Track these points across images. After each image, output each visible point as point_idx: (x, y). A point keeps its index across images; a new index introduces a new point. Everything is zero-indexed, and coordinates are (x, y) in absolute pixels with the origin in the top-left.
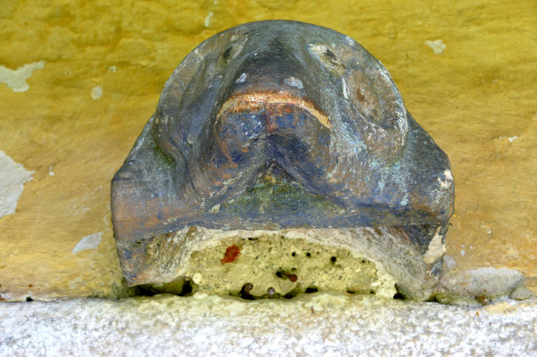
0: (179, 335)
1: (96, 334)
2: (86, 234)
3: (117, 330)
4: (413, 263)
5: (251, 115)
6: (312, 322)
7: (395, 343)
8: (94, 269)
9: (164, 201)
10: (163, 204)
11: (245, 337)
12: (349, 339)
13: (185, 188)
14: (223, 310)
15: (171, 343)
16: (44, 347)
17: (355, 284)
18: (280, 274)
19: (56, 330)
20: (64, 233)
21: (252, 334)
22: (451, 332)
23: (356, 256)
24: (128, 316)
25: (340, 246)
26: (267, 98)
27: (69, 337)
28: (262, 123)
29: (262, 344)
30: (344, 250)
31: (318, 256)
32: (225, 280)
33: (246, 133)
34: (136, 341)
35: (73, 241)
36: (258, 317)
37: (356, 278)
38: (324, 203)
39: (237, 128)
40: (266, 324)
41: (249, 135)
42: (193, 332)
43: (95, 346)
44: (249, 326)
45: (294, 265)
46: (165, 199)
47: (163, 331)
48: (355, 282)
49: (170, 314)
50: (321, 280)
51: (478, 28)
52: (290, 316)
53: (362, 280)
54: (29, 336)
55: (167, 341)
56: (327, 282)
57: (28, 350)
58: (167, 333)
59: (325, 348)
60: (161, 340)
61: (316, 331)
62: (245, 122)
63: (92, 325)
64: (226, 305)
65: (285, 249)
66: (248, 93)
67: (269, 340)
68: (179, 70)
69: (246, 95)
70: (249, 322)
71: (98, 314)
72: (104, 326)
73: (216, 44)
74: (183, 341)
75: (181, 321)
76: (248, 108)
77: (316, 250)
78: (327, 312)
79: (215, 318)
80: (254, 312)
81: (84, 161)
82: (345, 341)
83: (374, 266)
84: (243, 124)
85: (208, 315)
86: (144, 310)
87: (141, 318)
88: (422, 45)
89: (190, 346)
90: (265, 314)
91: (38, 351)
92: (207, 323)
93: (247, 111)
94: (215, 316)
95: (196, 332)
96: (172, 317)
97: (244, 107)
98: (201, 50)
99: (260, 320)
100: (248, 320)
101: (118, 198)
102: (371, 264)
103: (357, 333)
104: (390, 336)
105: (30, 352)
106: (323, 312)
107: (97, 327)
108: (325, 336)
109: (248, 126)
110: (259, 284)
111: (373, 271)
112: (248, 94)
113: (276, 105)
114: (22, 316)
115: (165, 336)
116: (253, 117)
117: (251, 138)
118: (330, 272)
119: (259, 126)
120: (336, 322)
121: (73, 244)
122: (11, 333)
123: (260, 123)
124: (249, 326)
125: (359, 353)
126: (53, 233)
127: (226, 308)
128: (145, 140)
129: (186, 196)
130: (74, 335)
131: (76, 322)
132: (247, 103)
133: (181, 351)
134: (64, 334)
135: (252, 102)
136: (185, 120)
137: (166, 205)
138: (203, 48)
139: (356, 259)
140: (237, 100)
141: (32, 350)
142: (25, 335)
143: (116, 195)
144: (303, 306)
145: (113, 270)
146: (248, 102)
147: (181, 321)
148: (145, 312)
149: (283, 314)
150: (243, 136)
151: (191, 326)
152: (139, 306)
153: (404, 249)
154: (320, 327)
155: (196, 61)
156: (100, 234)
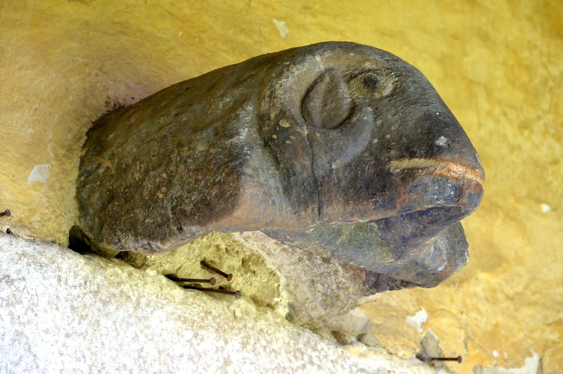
0: (140, 313)
1: (76, 292)
2: (37, 163)
3: (91, 292)
4: (341, 298)
5: (449, 183)
6: (232, 328)
7: (290, 367)
8: (47, 208)
9: (280, 211)
10: (278, 213)
11: (187, 329)
12: (259, 353)
13: (308, 207)
14: (170, 294)
15: (133, 320)
16: (37, 295)
17: (259, 294)
18: (205, 264)
19: (44, 278)
20: (17, 155)
21: (192, 327)
22: (326, 367)
23: (269, 266)
24: (99, 279)
25: (257, 251)
26: (466, 171)
27: (54, 289)
28: (455, 193)
29: (199, 341)
30: (259, 257)
31: (236, 255)
32: (169, 260)
33: (436, 197)
34: (107, 310)
35: (27, 168)
36: (196, 310)
37: (260, 287)
38: (383, 248)
39: (430, 189)
40: (203, 319)
41: (437, 199)
42: (149, 312)
43: (75, 305)
44: (190, 318)
45: (214, 257)
46: (281, 210)
47: (127, 304)
48: (259, 291)
49: (131, 286)
50: (237, 283)
51: (313, 20)
52: (219, 316)
53: (265, 291)
54: (24, 279)
55: (131, 316)
56: (242, 286)
57: (23, 295)
58: (130, 306)
59: (244, 359)
60: (126, 315)
61: (237, 338)
62: (440, 187)
63: (71, 282)
64: (171, 289)
65: (214, 240)
66: (453, 161)
67: (205, 337)
68: (299, 72)
69: (451, 163)
70: (190, 314)
71: (75, 269)
72: (80, 285)
73: (342, 61)
74: (142, 321)
75: (140, 297)
76: (449, 175)
77: (237, 249)
78: (245, 320)
79: (164, 302)
80: (193, 303)
81: (17, 66)
82: (257, 355)
83: (278, 280)
84: (437, 188)
85: (159, 296)
86: (111, 276)
87: (109, 284)
88: (271, 23)
89: (147, 327)
90: (201, 308)
91: (32, 298)
92: (159, 305)
93: (447, 178)
94: (166, 299)
95: (152, 312)
96: (133, 291)
97: (445, 173)
98: (324, 60)
99: (198, 314)
100: (189, 311)
101: (246, 195)
102: (275, 277)
103: (265, 347)
104: (286, 359)
105: (26, 298)
106: (242, 319)
107: (75, 284)
108: (244, 345)
109: (441, 191)
110: (190, 272)
111: (276, 285)
112: (453, 162)
113: (470, 181)
114: (14, 252)
115: (128, 311)
116: (450, 185)
117: (438, 202)
118: (245, 276)
119: (451, 195)
120: (251, 332)
121: (27, 171)
122: (7, 270)
123: (452, 193)
124: (190, 318)
125: (267, 371)
126: (8, 151)
127: (172, 292)
128: (249, 131)
129: (303, 213)
130: (59, 288)
131: (60, 273)
132: (449, 171)
133: (142, 332)
134: (51, 284)
135: (454, 172)
136: (338, 145)
137: (280, 214)
138: (326, 58)
139: (268, 269)
140: (442, 164)
141: (27, 295)
142: (20, 276)
143: (244, 192)
144: (228, 307)
145: (63, 214)
146: (451, 171)
147: (140, 297)
148: (112, 278)
149: (214, 313)
150: (431, 198)
151: (148, 305)
152: (106, 269)
153: (345, 283)
154: (241, 335)
155: (316, 68)
156: (47, 165)
